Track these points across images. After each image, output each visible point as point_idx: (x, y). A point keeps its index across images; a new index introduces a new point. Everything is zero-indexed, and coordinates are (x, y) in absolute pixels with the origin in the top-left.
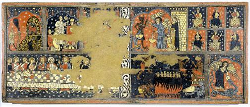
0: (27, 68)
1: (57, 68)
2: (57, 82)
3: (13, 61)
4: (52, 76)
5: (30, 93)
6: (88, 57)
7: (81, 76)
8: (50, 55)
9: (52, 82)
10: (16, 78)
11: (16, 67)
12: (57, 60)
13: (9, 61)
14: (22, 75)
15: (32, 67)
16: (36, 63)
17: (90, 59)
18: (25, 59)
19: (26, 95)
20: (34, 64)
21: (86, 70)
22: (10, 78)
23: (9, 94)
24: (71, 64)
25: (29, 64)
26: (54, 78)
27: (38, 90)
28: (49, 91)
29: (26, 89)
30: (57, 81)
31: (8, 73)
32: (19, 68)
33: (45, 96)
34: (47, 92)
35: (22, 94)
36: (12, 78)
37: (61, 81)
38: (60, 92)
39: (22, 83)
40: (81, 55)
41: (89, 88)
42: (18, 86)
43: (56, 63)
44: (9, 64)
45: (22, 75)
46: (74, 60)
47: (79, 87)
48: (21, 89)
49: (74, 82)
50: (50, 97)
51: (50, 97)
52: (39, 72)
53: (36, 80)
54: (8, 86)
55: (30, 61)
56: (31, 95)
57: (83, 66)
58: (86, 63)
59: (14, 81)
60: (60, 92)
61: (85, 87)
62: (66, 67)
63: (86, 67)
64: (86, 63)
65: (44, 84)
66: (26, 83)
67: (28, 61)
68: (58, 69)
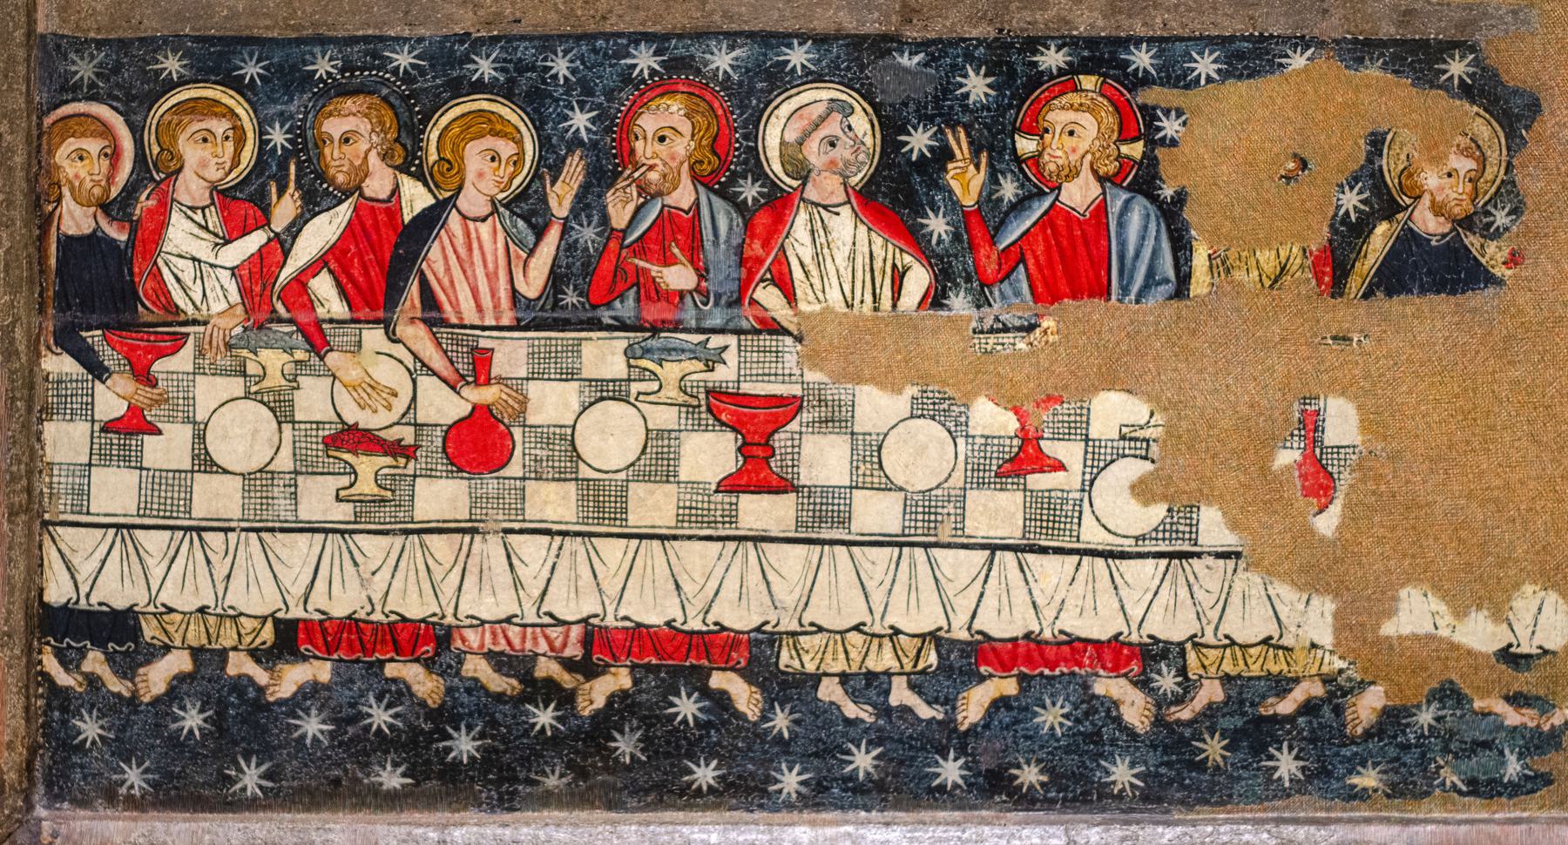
0: (384, 265)
1: (918, 280)
2: (927, 529)
3: (156, 170)
4: (836, 419)
5: (444, 717)
6: (1485, 91)
7: (1342, 423)
8: (798, 57)
9: (823, 525)
10: (205, 463)
11: (197, 263)
12: (919, 141)
13: (83, 164)
14: (313, 400)
15: (477, 265)
16: (561, 197)
17: (1512, 110)
18: (352, 134)
19: (384, 743)
20: (526, 206)
21: (1427, 318)
22: (101, 457)
23: (90, 728)
24: (1172, 214)
25: (430, 220)
26: (869, 453)
27: (587, 668)
28: (791, 688)
29: (361, 642)
30: (259, 479)
31: (59, 364)
32: (256, 278)
33: (705, 774)
34: (744, 696)
35: (313, 726)
36: (131, 459)
37: (998, 512)
38: (974, 705)
39: (298, 552)
40: (1359, 50)
41: (1480, 634)
42: (238, 598)
43: (894, 196)
44: (75, 219)
45: (313, 400)
46: (1225, 136)
47: (1314, 622)
48: (289, 638)
49: (1213, 528)
50: (790, 781)
51: (790, 781)
52: (604, 355)
53: (554, 502)
54: (57, 591)
55: (452, 166)
56: (464, 745)
57: (1381, 237)
58: (1441, 187)
59: (169, 514)
60: (974, 705)
61: (1416, 614)
62: (1073, 263)
63: (1439, 268)
64: (1441, 187)
65: (698, 558)
66: (372, 547)
67: (410, 164)
68: (935, 299)
